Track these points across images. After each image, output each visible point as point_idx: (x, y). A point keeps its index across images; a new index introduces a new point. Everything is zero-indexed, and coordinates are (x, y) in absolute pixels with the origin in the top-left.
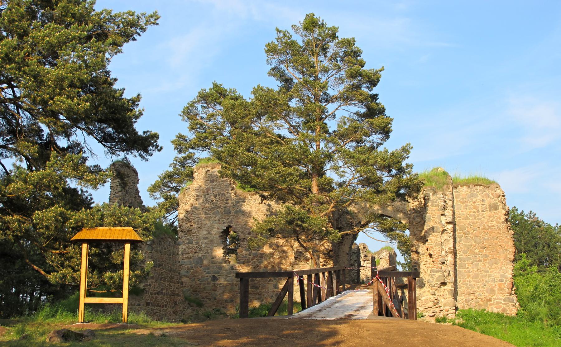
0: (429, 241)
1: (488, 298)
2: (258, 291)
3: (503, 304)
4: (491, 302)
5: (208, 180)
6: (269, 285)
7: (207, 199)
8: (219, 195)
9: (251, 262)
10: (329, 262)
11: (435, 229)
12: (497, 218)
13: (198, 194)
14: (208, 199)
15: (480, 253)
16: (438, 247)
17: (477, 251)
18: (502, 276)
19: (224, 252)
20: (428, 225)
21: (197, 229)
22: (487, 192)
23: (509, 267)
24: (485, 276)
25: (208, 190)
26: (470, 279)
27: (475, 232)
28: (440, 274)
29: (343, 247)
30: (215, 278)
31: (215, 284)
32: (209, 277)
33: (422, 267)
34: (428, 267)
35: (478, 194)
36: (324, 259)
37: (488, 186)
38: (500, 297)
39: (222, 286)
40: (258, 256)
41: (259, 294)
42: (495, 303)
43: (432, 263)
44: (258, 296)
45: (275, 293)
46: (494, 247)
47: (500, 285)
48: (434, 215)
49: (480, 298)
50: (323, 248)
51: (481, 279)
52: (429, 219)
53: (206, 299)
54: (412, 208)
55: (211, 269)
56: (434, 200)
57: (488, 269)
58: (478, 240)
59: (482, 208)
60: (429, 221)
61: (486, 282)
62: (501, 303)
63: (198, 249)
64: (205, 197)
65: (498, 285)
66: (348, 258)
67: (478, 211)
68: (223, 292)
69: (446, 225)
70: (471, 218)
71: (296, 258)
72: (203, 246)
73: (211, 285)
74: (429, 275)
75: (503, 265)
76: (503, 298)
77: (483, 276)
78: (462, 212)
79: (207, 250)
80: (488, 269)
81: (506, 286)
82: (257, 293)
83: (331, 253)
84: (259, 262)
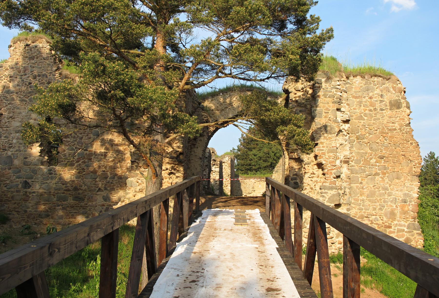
0: (320, 145)
1: (387, 224)
2: (83, 204)
3: (406, 232)
4: (390, 229)
5: (27, 57)
6: (98, 197)
7: (23, 80)
8: (39, 76)
9: (76, 164)
10: (177, 169)
11: (328, 128)
12: (400, 119)
13: (12, 73)
14: (25, 80)
15: (378, 164)
16: (332, 154)
17: (373, 161)
18: (405, 195)
19: (41, 150)
20: (319, 121)
21: (8, 119)
22: (387, 85)
23: (414, 184)
24: (384, 194)
25: (25, 69)
26: (363, 197)
27: (371, 136)
28: (333, 192)
29: (195, 149)
30: (26, 185)
31: (26, 192)
32: (19, 183)
33: (306, 180)
34: (317, 182)
35: (375, 87)
36: (172, 165)
37: (388, 77)
38: (403, 223)
39: (37, 195)
40: (84, 158)
41: (84, 208)
42: (396, 231)
43: (321, 176)
44: (82, 211)
45: (105, 207)
46: (395, 157)
47: (402, 207)
48: (327, 109)
49: (377, 224)
50: (170, 150)
51: (378, 199)
52: (321, 114)
53: (13, 212)
54: (294, 99)
55: (23, 172)
56: (327, 88)
57: (388, 185)
58: (374, 146)
59: (380, 106)
60: (320, 117)
61: (384, 202)
62: (404, 230)
63: (7, 145)
64: (21, 78)
65: (400, 206)
66: (201, 164)
67: (375, 109)
68: (38, 203)
69: (341, 124)
70: (366, 118)
71: (132, 162)
72: (15, 141)
73: (21, 194)
74: (318, 193)
75: (406, 181)
76: (406, 224)
77: (381, 195)
78: (354, 109)
79: (19, 147)
80: (388, 185)
81: (411, 209)
82: (81, 206)
83: (181, 157)
84: (86, 166)
